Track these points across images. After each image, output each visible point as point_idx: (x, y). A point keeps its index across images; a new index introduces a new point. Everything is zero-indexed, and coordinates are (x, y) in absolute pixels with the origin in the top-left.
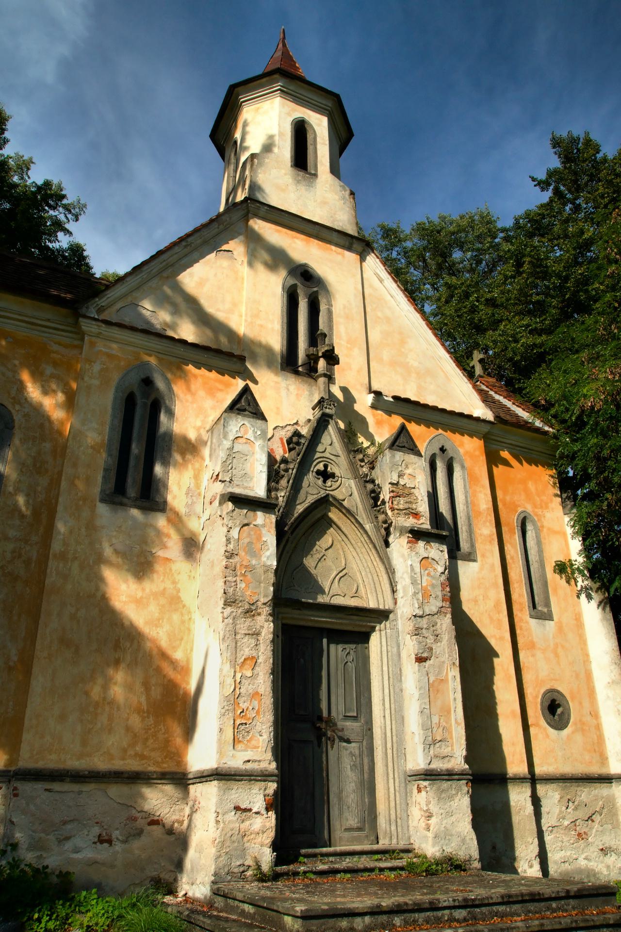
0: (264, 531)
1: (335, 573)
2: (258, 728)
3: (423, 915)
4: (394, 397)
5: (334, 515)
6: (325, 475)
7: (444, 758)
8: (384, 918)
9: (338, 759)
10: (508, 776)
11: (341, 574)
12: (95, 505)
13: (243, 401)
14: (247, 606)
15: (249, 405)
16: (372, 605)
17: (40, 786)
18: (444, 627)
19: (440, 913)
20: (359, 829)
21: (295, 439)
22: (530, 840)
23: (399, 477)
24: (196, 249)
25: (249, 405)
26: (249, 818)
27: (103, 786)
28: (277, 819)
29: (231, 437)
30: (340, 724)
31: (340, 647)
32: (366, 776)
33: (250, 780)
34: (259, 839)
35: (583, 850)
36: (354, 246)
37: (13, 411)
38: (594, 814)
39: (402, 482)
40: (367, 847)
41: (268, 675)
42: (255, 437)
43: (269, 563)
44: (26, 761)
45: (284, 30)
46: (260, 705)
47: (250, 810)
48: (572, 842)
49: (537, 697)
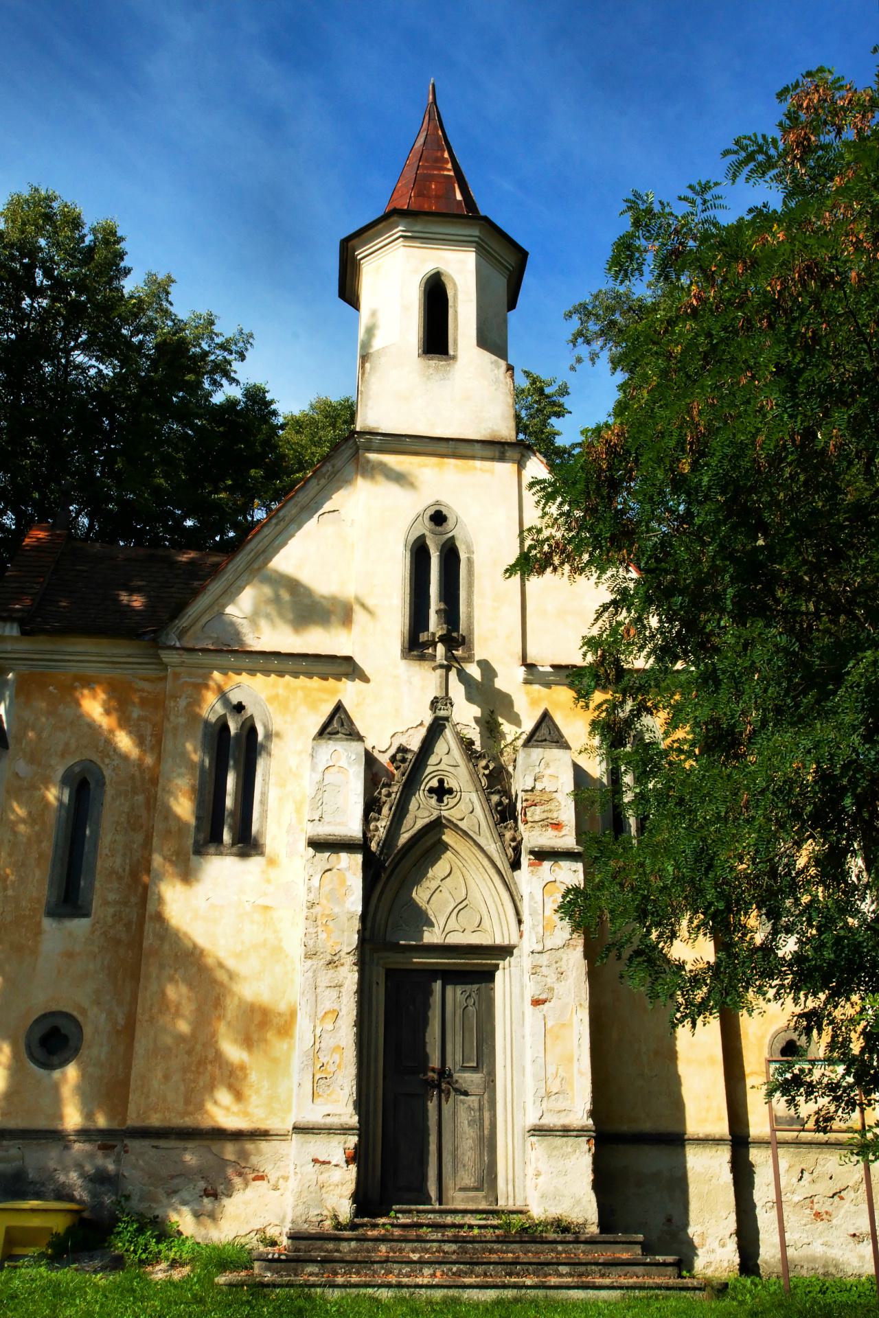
0: (349, 875)
1: (453, 905)
3: (410, 1245)
4: (553, 666)
5: (448, 837)
6: (441, 792)
7: (559, 1112)
8: (370, 1244)
9: (454, 1113)
12: (189, 859)
13: (335, 722)
14: (329, 958)
15: (342, 725)
17: (147, 1143)
18: (571, 963)
19: (428, 1245)
20: (476, 1189)
21: (399, 756)
23: (535, 780)
25: (342, 725)
26: (328, 1170)
29: (321, 769)
30: (456, 1076)
31: (459, 989)
32: (486, 1132)
33: (329, 1134)
34: (338, 1191)
35: (821, 1233)
36: (508, 454)
37: (102, 766)
38: (844, 1190)
39: (539, 787)
41: (351, 1027)
42: (349, 764)
43: (353, 909)
44: (133, 1120)
46: (341, 1059)
47: (329, 1163)
48: (803, 1222)
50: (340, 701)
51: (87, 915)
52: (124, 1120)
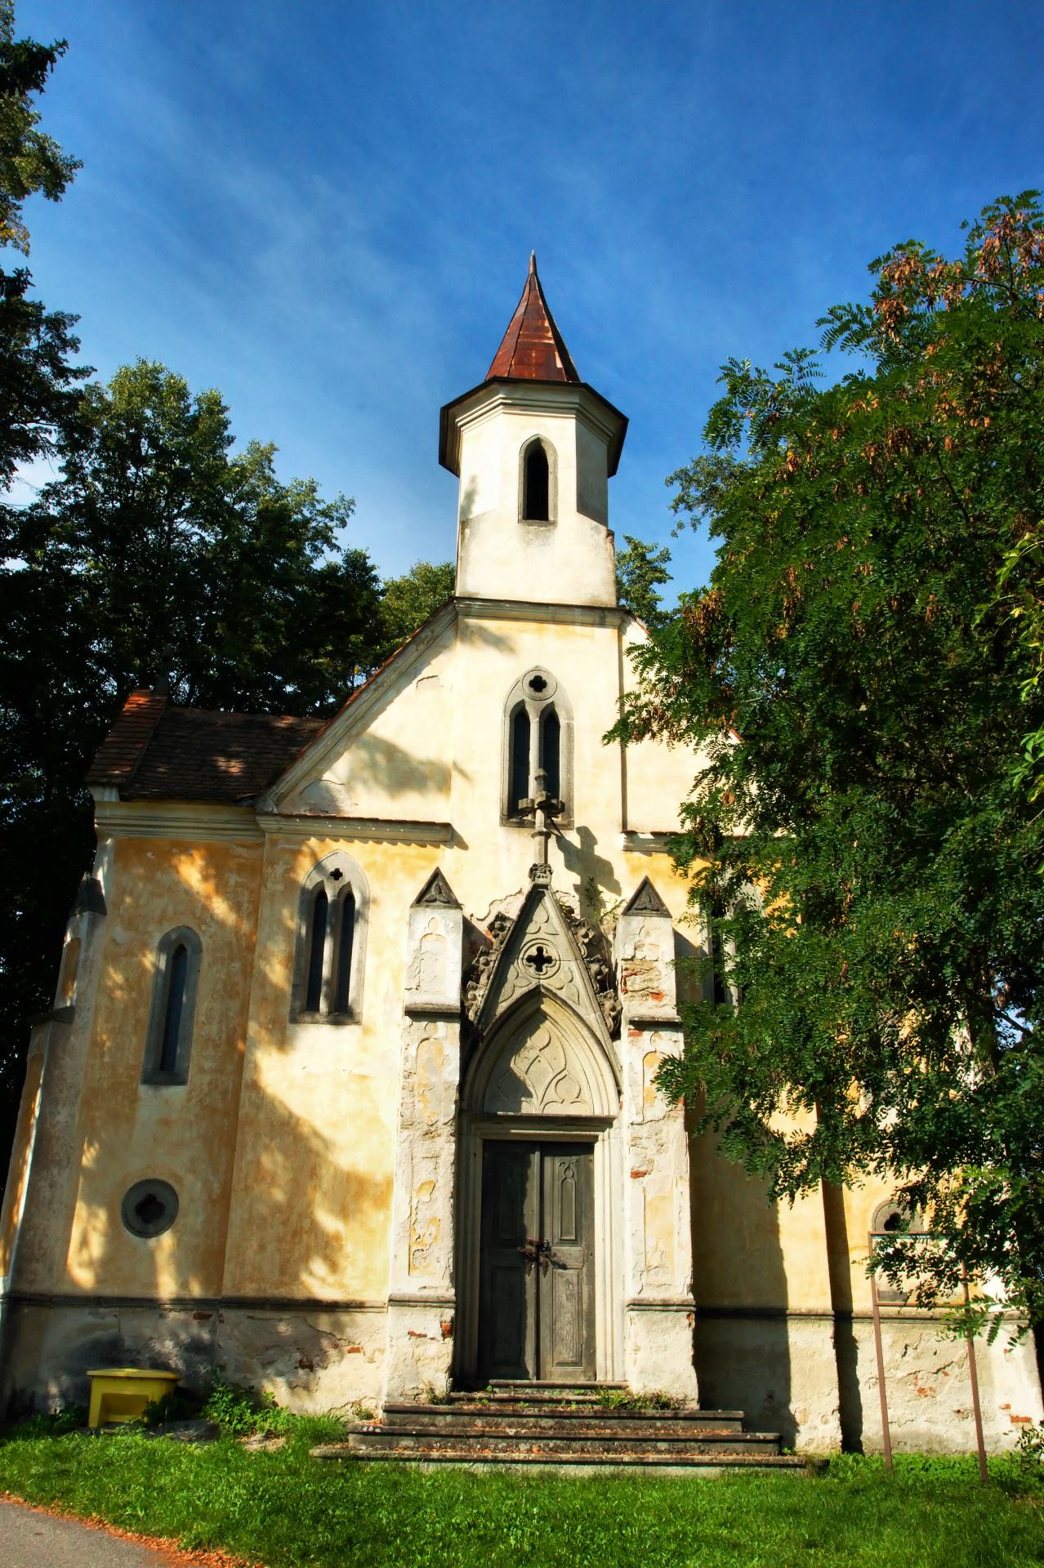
0: (446, 1044)
1: (552, 1076)
2: (436, 1254)
4: (653, 834)
5: (547, 1006)
6: (540, 960)
7: (659, 1286)
8: (466, 1419)
9: (552, 1287)
10: (788, 1312)
11: (559, 1077)
13: (433, 889)
14: (426, 1128)
15: (440, 893)
16: (598, 1113)
18: (672, 1134)
19: (525, 1420)
20: (574, 1364)
22: (827, 1391)
24: (390, 687)
25: (440, 893)
27: (301, 1314)
28: (455, 1345)
29: (420, 937)
30: (554, 1249)
31: (558, 1161)
34: (434, 1364)
36: (608, 620)
37: (200, 934)
40: (582, 1381)
42: (447, 932)
44: (228, 1291)
45: (534, 257)
47: (425, 1336)
48: (907, 1398)
49: (866, 1211)
50: (438, 869)
51: (183, 1082)
52: (219, 1290)
